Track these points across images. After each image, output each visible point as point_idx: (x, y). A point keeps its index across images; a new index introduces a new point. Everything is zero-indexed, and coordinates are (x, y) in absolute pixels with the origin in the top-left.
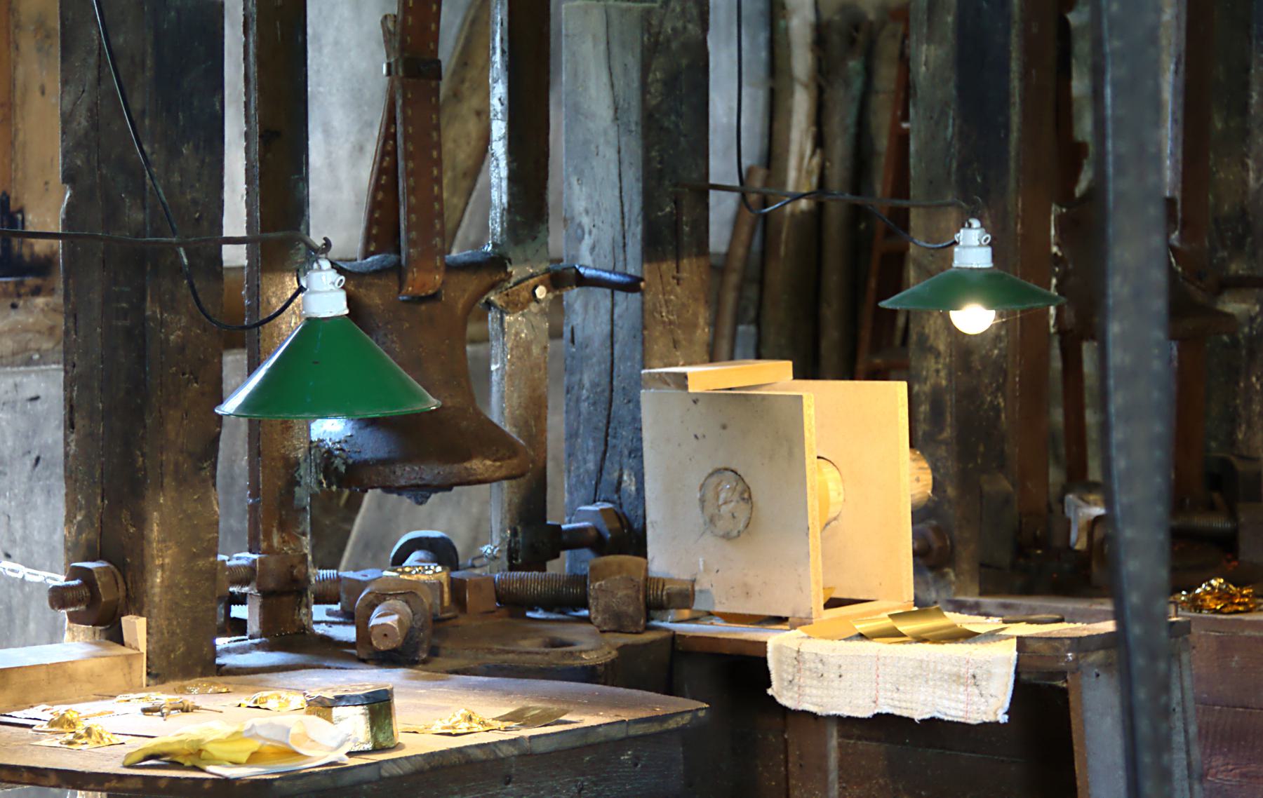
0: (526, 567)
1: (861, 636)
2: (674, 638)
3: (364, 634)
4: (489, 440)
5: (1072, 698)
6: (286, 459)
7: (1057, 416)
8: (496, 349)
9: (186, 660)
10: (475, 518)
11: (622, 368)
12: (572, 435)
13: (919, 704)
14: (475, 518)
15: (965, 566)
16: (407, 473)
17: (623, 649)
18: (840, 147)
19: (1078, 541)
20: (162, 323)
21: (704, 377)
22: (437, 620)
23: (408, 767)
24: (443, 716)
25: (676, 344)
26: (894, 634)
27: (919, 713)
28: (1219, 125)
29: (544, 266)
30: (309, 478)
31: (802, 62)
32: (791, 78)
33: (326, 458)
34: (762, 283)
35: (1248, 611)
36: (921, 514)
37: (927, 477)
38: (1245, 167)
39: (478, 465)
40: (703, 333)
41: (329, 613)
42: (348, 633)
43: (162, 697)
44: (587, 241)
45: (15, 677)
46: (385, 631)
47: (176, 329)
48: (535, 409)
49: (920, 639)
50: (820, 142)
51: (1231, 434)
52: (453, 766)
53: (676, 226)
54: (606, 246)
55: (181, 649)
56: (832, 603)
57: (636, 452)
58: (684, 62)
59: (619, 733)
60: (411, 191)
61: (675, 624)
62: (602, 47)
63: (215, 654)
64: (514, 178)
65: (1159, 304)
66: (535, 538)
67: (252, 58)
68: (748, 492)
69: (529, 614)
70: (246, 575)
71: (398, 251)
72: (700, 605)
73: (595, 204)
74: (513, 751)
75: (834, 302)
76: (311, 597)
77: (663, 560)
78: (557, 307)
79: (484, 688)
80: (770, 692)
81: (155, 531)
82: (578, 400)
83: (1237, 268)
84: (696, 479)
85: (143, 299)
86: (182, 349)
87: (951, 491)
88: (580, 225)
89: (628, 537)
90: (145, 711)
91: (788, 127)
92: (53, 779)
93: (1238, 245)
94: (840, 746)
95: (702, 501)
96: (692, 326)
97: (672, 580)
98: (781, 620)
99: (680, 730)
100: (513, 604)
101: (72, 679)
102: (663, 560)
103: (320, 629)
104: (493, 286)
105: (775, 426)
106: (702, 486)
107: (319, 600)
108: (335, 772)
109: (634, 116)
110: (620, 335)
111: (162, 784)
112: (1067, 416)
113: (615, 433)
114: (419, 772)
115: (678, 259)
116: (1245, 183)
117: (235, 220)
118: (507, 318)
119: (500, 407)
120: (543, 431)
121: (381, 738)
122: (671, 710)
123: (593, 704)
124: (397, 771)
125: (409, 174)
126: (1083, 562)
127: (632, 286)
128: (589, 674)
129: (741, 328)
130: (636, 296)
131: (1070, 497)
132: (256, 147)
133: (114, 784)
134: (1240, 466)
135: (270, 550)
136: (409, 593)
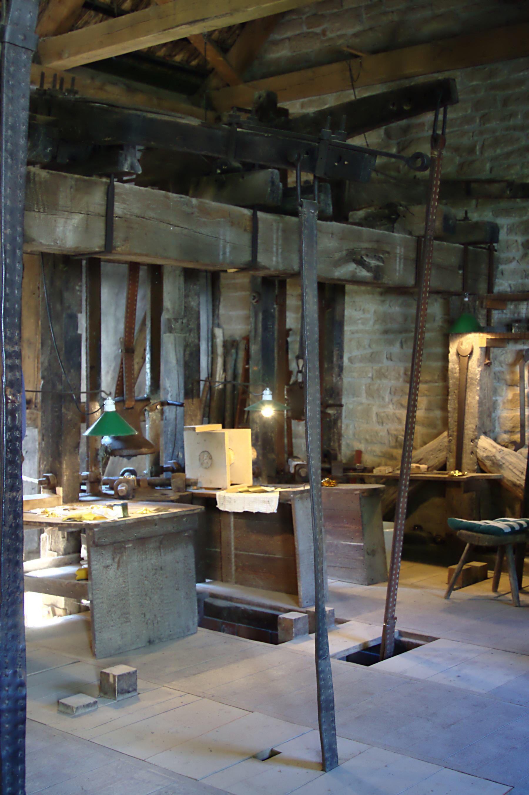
0: (156, 476)
1: (240, 492)
2: (193, 494)
3: (117, 493)
4: (146, 444)
5: (292, 506)
6: (96, 449)
7: (286, 441)
8: (147, 421)
9: (72, 498)
10: (144, 464)
11: (178, 426)
12: (166, 443)
13: (254, 508)
14: (144, 464)
15: (264, 477)
16: (125, 452)
17: (180, 496)
18: (230, 372)
19: (292, 471)
20: (66, 414)
21: (200, 428)
22: (134, 489)
23: (132, 521)
24: (140, 510)
25: (192, 420)
26: (248, 491)
27: (255, 511)
28: (326, 366)
29: (159, 400)
30: (101, 453)
31: (220, 350)
32: (217, 355)
33: (106, 448)
34: (209, 407)
35: (335, 486)
36: (254, 463)
37: (255, 453)
38: (332, 376)
39: (144, 450)
40: (199, 417)
41: (106, 488)
42: (112, 492)
43: (66, 507)
44: (170, 394)
45: (31, 502)
46: (122, 491)
47: (69, 415)
48: (157, 436)
49: (255, 492)
50: (225, 370)
51: (329, 444)
52: (143, 521)
53: (192, 391)
54: (175, 395)
55: (71, 496)
56: (232, 485)
57: (183, 447)
58: (194, 349)
59: (183, 514)
60: (127, 381)
61: (193, 490)
62: (174, 345)
63: (79, 497)
64: (152, 378)
65: (318, 402)
66: (157, 469)
67: (88, 348)
68: (211, 455)
69: (156, 488)
70: (87, 478)
71: (123, 396)
72: (199, 485)
73: (172, 385)
74: (157, 517)
75: (232, 410)
76: (102, 483)
77: (189, 474)
78: (162, 412)
79: (148, 504)
80: (217, 506)
81: (64, 466)
82: (167, 434)
83: (331, 402)
84: (198, 454)
85: (62, 408)
86: (71, 420)
87: (260, 458)
88: (168, 390)
89: (182, 469)
90: (64, 510)
91: (216, 367)
92: (45, 524)
93: (331, 396)
94: (234, 521)
95: (200, 459)
96: (196, 416)
97: (192, 479)
98: (219, 489)
99: (198, 513)
100: (152, 485)
101: (44, 502)
102: (189, 474)
103: (104, 492)
104: (147, 405)
105: (219, 440)
106: (200, 455)
107: (104, 484)
108: (115, 522)
109: (182, 362)
110: (178, 418)
111: (72, 525)
112: (288, 441)
113: (177, 443)
114: (135, 522)
115: (193, 398)
116: (332, 380)
117: (84, 387)
118: (150, 413)
119: (148, 436)
120: (159, 442)
121: (125, 514)
122: (195, 508)
123: (175, 507)
124: (130, 522)
125: (126, 377)
126: (293, 475)
127: (182, 405)
128: (172, 501)
129: (205, 418)
130: (182, 408)
131: (290, 460)
132: (89, 370)
133: (60, 525)
134: (332, 452)
135: (92, 471)
136: (127, 482)
